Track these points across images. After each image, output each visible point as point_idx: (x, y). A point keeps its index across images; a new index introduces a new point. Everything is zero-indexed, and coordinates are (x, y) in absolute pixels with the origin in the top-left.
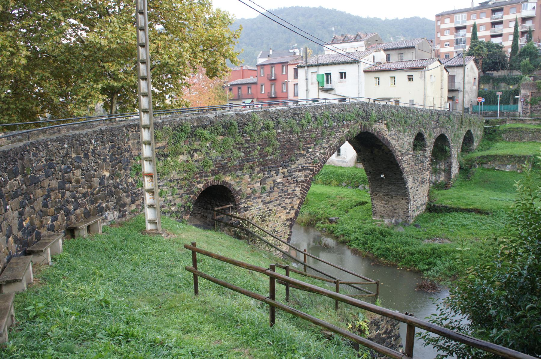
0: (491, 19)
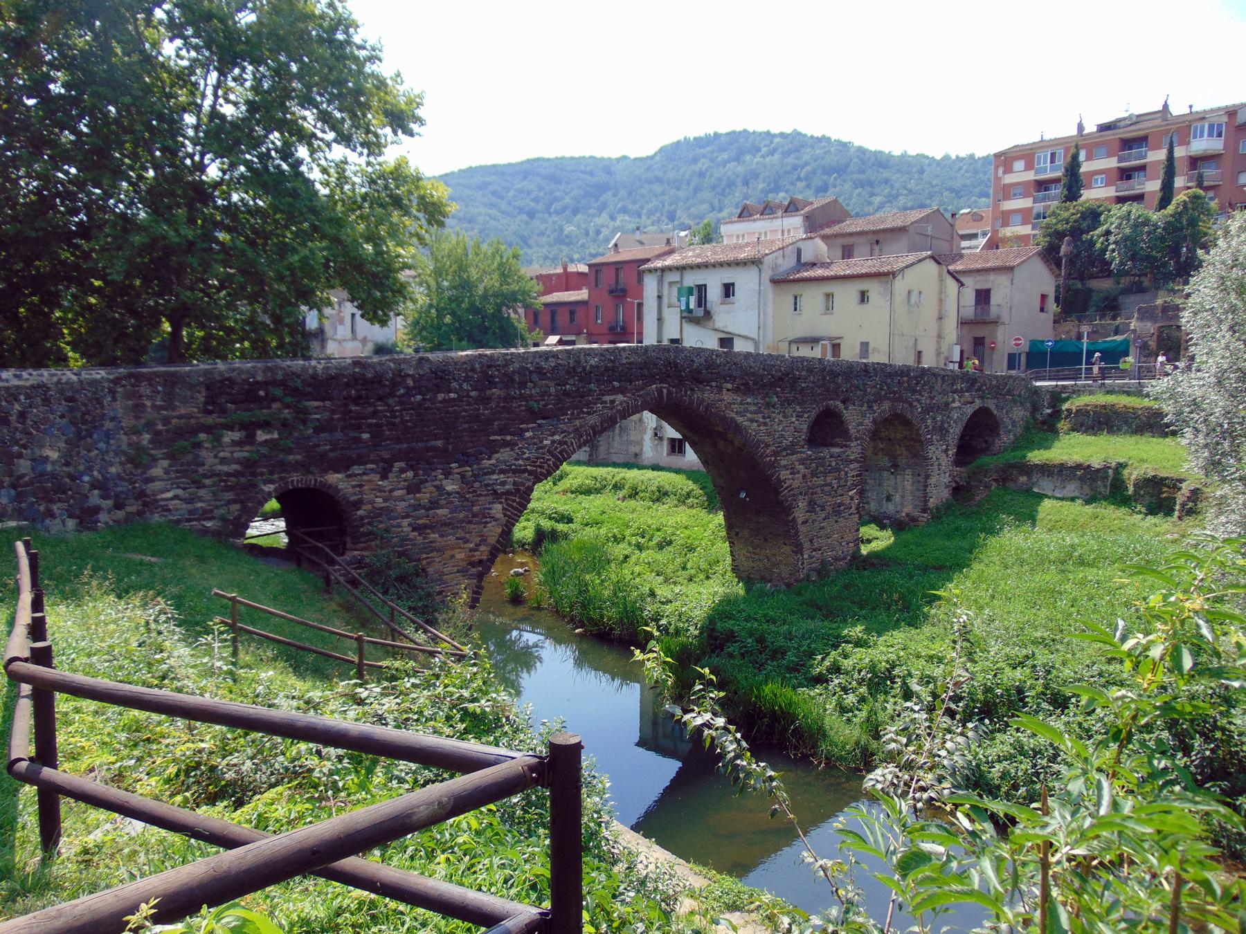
0: (1120, 161)
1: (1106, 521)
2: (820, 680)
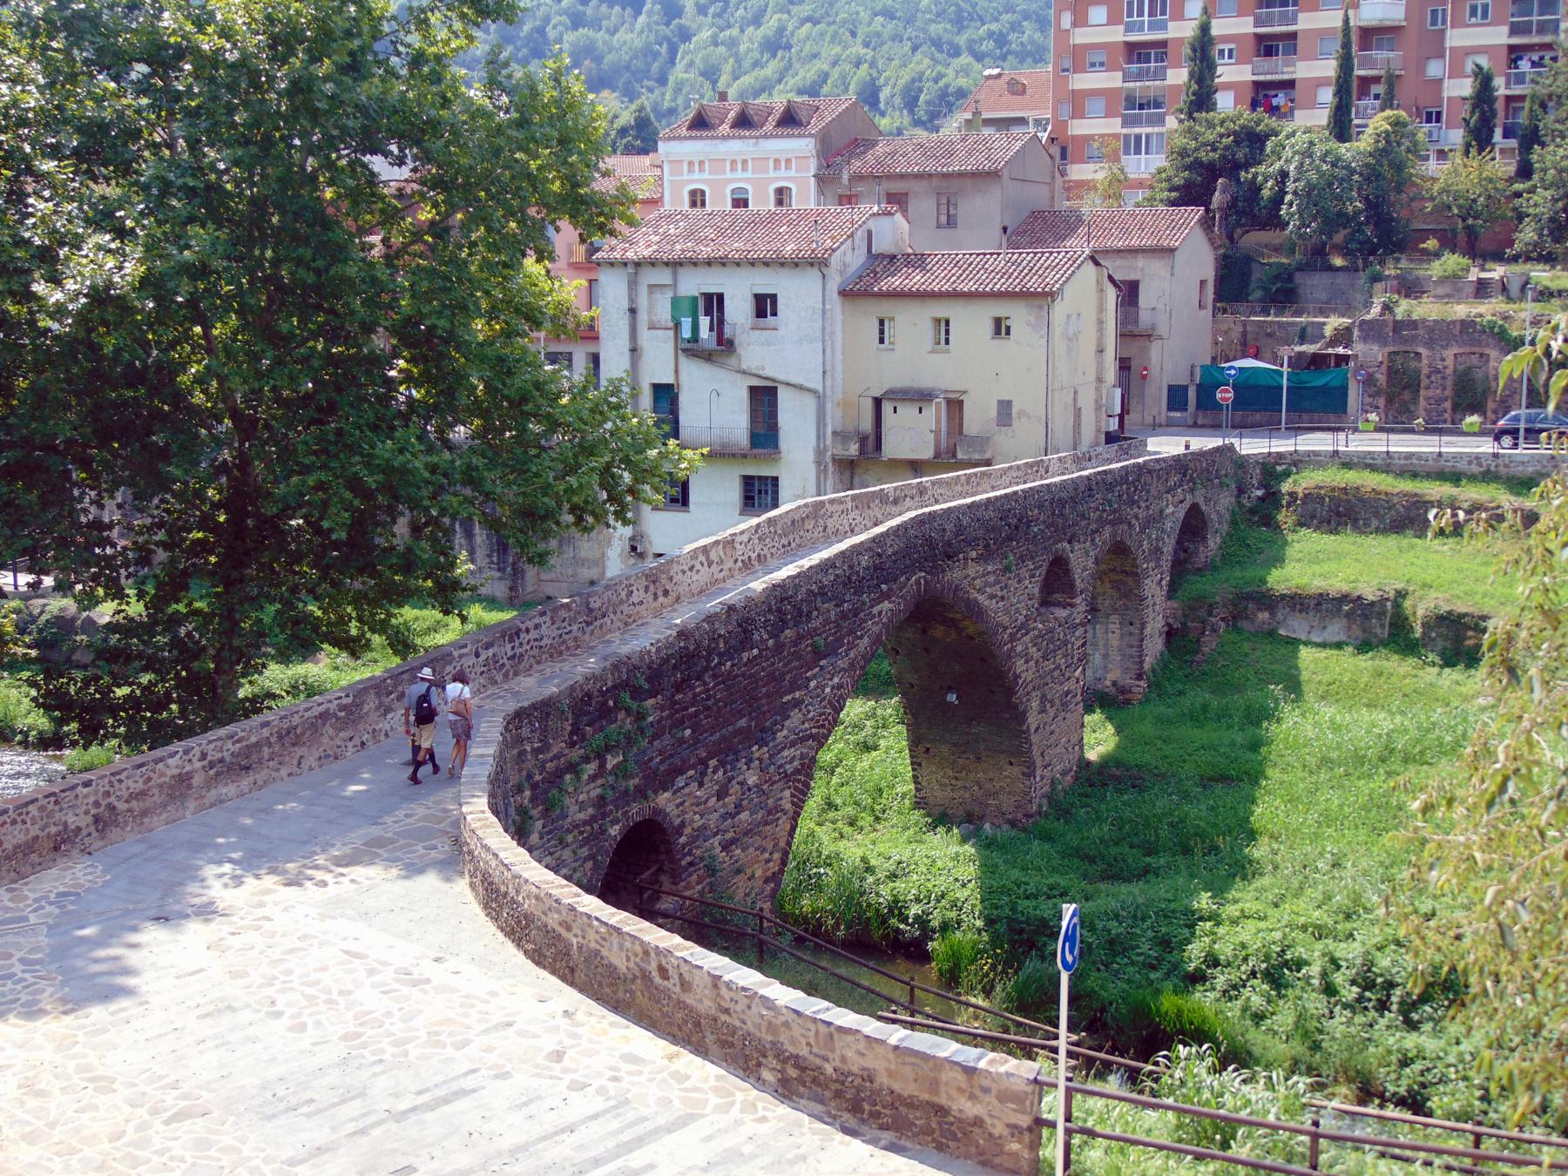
1: (1394, 679)
2: (1197, 978)
